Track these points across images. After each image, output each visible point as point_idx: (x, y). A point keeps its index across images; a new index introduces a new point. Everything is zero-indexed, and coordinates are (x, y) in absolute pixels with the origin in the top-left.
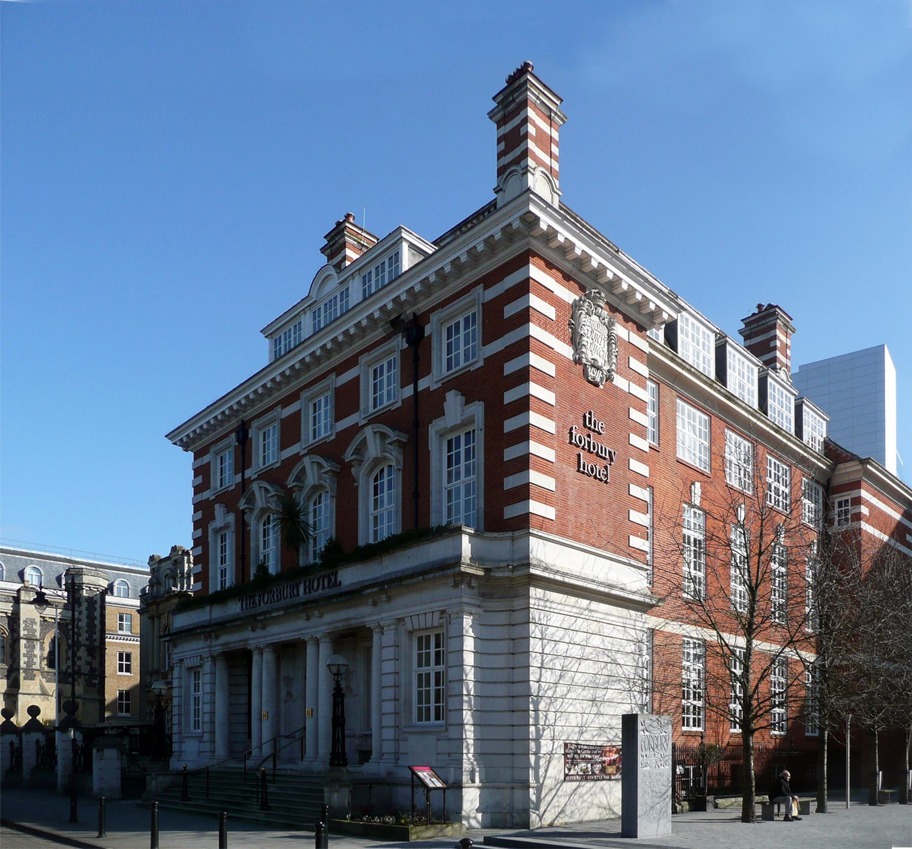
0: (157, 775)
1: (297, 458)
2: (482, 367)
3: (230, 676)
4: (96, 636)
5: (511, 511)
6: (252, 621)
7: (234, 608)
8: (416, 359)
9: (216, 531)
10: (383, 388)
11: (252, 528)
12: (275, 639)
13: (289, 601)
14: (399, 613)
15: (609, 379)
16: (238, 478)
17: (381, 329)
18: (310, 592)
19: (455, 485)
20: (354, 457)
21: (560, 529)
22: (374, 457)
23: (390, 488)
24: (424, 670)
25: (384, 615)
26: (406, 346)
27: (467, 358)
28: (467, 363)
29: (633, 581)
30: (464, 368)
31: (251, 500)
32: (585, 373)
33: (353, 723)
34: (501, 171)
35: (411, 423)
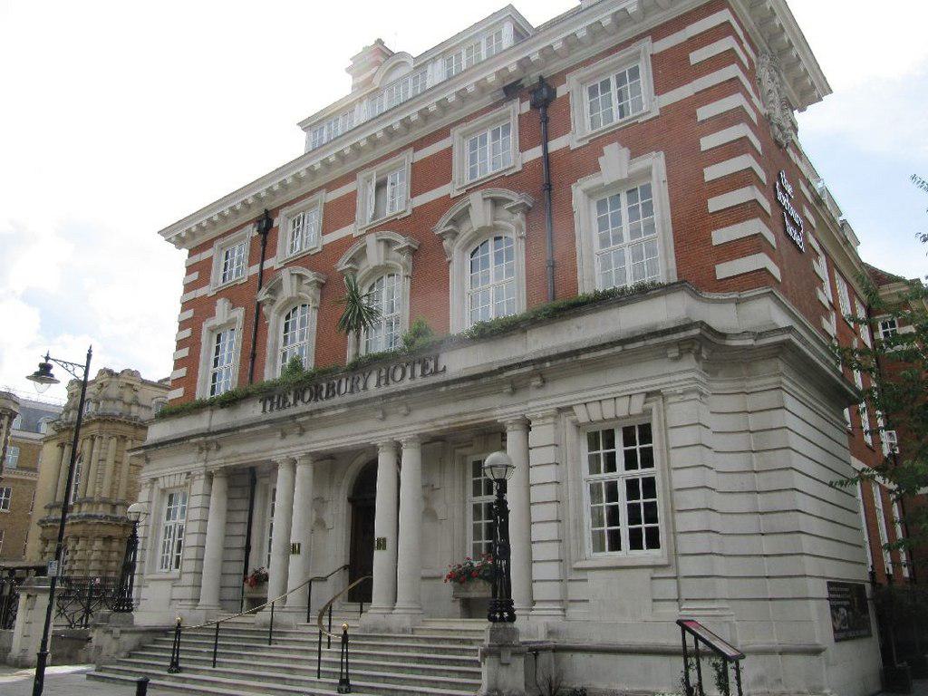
0: (122, 632)
2: (657, 117)
3: (230, 499)
8: (265, 243)
12: (233, 462)
13: (349, 398)
14: (154, 474)
16: (255, 269)
17: (489, 97)
18: (387, 383)
20: (348, 266)
23: (302, 325)
24: (647, 472)
25: (531, 405)
26: (256, 234)
27: (237, 274)
28: (636, 114)
30: (633, 119)
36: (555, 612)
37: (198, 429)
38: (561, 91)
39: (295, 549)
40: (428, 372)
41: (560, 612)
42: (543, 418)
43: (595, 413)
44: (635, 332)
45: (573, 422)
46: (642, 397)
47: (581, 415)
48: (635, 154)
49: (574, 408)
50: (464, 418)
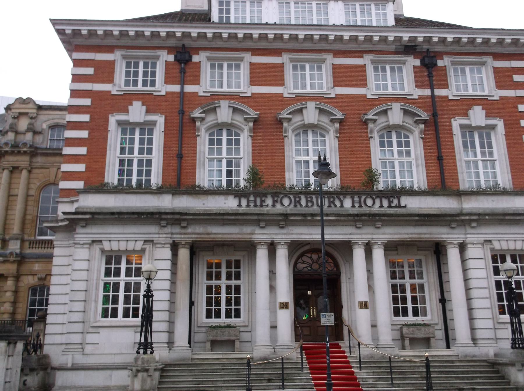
25: (468, 236)
36: (79, 350)
37: (504, 208)
38: (195, 58)
39: (364, 305)
40: (393, 205)
41: (81, 350)
42: (83, 244)
43: (115, 246)
44: (166, 209)
45: (100, 249)
46: (142, 242)
47: (107, 246)
48: (488, 116)
49: (103, 242)
50: (422, 236)
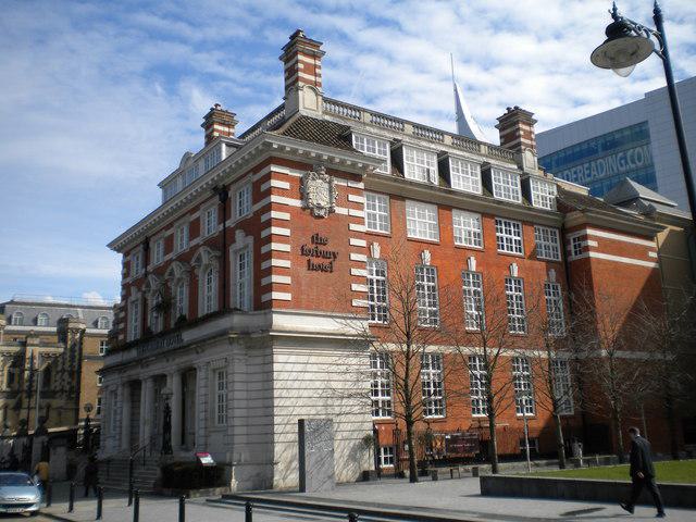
1: (198, 246)
4: (76, 364)
5: (264, 298)
6: (139, 362)
7: (133, 353)
9: (235, 252)
10: (211, 226)
11: (200, 278)
12: (151, 374)
14: (207, 359)
15: (331, 211)
19: (241, 280)
21: (297, 306)
22: (201, 264)
29: (356, 327)
31: (148, 286)
32: (312, 213)
33: (188, 426)
34: (287, 88)
35: (221, 244)
